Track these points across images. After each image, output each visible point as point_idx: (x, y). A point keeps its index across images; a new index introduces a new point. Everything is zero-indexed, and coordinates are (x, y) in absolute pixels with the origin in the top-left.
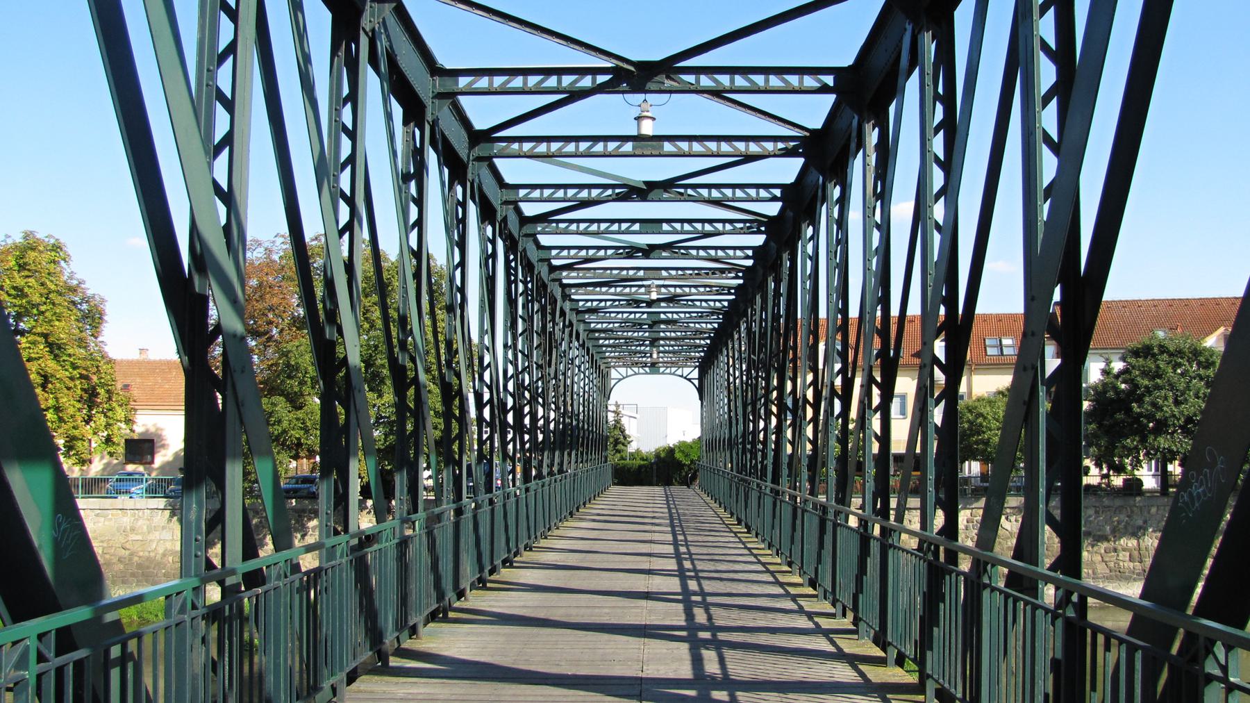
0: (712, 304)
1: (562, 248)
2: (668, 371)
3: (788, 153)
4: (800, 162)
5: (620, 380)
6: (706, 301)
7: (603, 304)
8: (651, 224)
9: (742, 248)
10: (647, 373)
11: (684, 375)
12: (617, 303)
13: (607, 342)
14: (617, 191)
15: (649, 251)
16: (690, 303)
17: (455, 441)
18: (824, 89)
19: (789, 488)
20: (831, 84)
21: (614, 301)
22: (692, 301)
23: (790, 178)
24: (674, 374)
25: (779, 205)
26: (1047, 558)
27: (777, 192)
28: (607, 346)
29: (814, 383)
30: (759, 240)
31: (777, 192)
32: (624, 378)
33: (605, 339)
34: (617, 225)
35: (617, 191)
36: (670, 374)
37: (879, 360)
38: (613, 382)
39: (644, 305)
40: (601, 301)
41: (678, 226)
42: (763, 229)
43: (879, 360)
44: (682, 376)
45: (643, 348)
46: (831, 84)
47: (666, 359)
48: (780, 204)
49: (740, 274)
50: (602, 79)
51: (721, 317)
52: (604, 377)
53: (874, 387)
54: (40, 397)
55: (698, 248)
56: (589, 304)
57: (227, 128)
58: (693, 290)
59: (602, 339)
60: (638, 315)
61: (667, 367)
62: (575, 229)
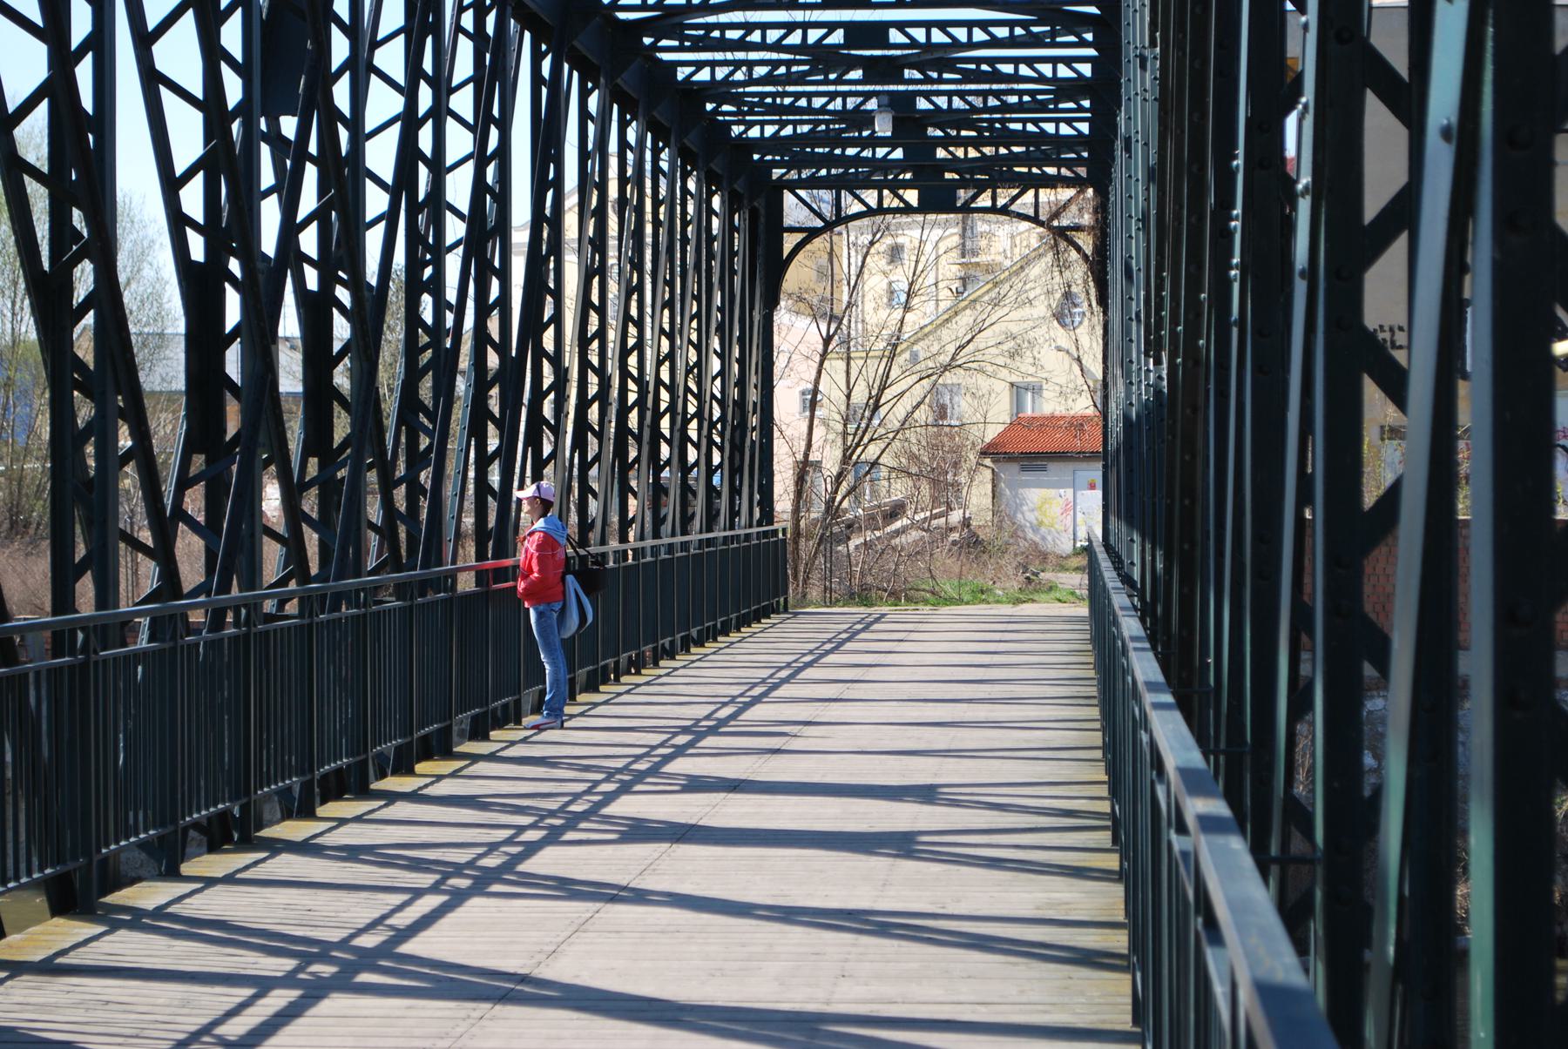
0: (919, 34)
2: (984, 201)
5: (812, 233)
6: (1030, 62)
10: (907, 209)
11: (1043, 217)
16: (984, 67)
17: (592, 459)
24: (1005, 211)
29: (658, 470)
32: (829, 226)
34: (799, 32)
36: (993, 210)
37: (1367, 792)
38: (790, 242)
43: (1367, 792)
44: (1035, 220)
52: (768, 226)
54: (83, 224)
57: (1401, 178)
60: (721, 73)
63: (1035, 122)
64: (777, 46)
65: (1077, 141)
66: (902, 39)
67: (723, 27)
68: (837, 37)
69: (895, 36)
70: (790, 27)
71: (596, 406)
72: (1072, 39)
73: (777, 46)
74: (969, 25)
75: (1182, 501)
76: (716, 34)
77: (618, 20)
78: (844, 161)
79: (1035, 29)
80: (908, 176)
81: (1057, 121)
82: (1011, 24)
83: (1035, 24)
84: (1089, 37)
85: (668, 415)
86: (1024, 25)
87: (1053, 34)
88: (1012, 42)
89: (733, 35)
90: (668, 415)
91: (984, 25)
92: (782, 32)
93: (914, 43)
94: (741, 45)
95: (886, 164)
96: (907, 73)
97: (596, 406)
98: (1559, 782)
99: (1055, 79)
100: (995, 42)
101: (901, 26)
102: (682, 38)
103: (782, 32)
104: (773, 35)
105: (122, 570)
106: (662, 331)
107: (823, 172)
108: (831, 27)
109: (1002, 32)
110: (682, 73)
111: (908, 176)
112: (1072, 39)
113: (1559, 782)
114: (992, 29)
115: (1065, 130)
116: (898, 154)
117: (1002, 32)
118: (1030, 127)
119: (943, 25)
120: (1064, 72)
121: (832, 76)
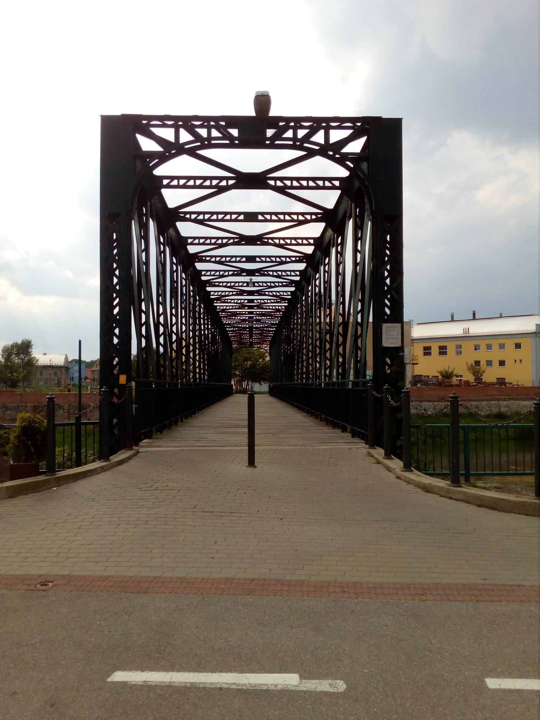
0: (277, 307)
1: (215, 292)
3: (317, 220)
4: (322, 225)
6: (275, 306)
7: (228, 308)
8: (251, 259)
9: (286, 292)
12: (234, 307)
13: (230, 329)
14: (235, 240)
15: (250, 273)
18: (334, 188)
19: (339, 423)
20: (290, 294)
21: (233, 306)
22: (268, 306)
23: (317, 235)
25: (313, 248)
26: (236, 369)
27: (298, 273)
28: (230, 331)
30: (293, 289)
31: (337, 183)
33: (229, 328)
34: (218, 272)
35: (235, 240)
39: (247, 308)
40: (227, 306)
41: (261, 284)
42: (294, 285)
45: (246, 337)
46: (290, 294)
47: (256, 337)
48: (339, 192)
49: (286, 302)
50: (231, 182)
51: (279, 318)
53: (319, 361)
55: (273, 271)
56: (222, 308)
58: (269, 301)
59: (228, 328)
61: (256, 345)
62: (222, 285)
63: (270, 321)
64: (236, 303)
65: (276, 324)
66: (257, 302)
68: (246, 301)
69: (255, 301)
70: (238, 300)
72: (284, 302)
73: (236, 303)
74: (267, 299)
76: (241, 313)
78: (239, 327)
79: (278, 300)
80: (244, 242)
81: (258, 325)
82: (274, 299)
83: (278, 299)
84: (286, 302)
86: (276, 299)
87: (281, 301)
88: (274, 302)
89: (229, 301)
91: (270, 300)
92: (215, 272)
93: (258, 302)
94: (230, 303)
100: (272, 303)
101: (256, 300)
102: (221, 301)
103: (215, 272)
104: (236, 301)
105: (40, 479)
107: (234, 329)
108: (245, 300)
109: (273, 301)
110: (218, 307)
111: (244, 242)
112: (284, 302)
114: (291, 258)
115: (259, 326)
116: (227, 329)
117: (273, 301)
119: (263, 300)
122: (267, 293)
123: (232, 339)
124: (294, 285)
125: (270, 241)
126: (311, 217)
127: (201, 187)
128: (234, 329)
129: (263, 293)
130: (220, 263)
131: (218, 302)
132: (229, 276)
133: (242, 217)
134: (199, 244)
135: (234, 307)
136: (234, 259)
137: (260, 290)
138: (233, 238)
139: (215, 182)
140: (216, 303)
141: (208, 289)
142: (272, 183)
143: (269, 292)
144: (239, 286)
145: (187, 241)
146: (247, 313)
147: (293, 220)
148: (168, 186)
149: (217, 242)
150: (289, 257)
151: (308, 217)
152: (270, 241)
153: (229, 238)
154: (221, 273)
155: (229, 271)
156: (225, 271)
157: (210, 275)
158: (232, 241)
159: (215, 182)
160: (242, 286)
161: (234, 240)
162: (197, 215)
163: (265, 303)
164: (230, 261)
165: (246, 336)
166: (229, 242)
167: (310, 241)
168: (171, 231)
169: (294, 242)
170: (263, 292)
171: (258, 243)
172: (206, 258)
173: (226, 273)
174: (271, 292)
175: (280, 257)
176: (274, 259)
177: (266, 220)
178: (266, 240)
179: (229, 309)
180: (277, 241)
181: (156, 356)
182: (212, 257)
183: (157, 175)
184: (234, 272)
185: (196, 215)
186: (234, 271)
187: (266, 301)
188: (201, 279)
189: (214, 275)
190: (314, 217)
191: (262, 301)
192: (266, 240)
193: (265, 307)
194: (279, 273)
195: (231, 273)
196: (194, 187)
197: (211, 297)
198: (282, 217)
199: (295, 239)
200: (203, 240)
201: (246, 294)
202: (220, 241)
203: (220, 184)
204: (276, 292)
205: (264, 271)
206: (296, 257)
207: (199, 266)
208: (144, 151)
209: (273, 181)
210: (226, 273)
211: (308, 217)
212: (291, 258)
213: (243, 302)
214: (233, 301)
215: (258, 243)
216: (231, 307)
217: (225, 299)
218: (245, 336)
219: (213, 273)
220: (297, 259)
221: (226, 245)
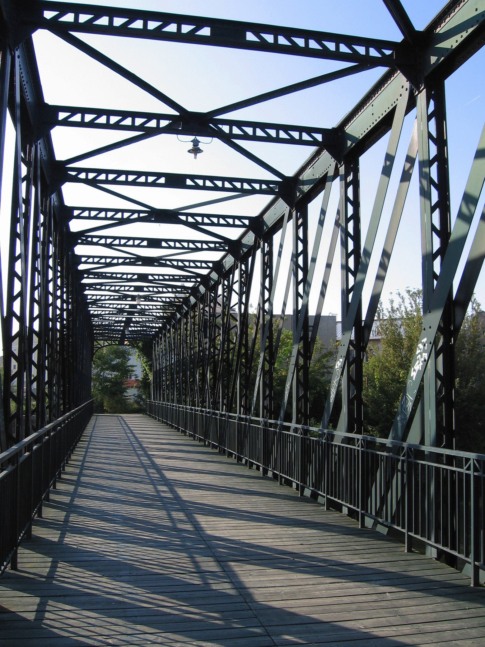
7: (103, 298)
35: (132, 260)
39: (130, 299)
45: (117, 335)
56: (94, 297)
58: (154, 307)
64: (116, 308)
67: (105, 304)
68: (128, 307)
71: (15, 381)
75: (183, 367)
77: (87, 302)
85: (15, 294)
89: (107, 305)
90: (15, 294)
93: (150, 291)
94: (108, 307)
95: (27, 365)
96: (135, 314)
97: (15, 381)
98: (38, 332)
99: (156, 316)
104: (115, 306)
106: (347, 199)
107: (104, 332)
108: (126, 305)
110: (89, 297)
113: (38, 332)
116: (95, 338)
118: (144, 324)
119: (148, 305)
120: (158, 315)
121: (121, 314)
122: (155, 299)
123: (94, 323)
124: (227, 248)
125: (168, 263)
126: (261, 187)
127: (117, 126)
128: (104, 332)
129: (150, 298)
130: (110, 246)
131: (90, 276)
132: (118, 264)
133: (145, 243)
134: (89, 218)
135: (112, 297)
136: (131, 243)
137: (148, 296)
138: (139, 212)
139: (139, 121)
140: (91, 307)
141: (86, 292)
142: (183, 218)
143: (157, 297)
144: (125, 291)
145: (57, 116)
146: (206, 31)
147: (235, 189)
148: (66, 123)
149: (116, 217)
150: (207, 243)
151: (257, 186)
152: (168, 263)
153: (133, 212)
154: (108, 260)
155: (118, 258)
156: (113, 258)
157: (93, 263)
158: (136, 216)
159: (139, 121)
160: (128, 291)
161: (139, 215)
162: (96, 122)
163: (150, 309)
164: (125, 245)
165: (117, 334)
166: (132, 217)
167: (209, 264)
168: (40, 144)
169: (192, 264)
170: (151, 297)
171: (155, 264)
172: (92, 240)
173: (115, 261)
174: (160, 297)
175: (193, 242)
176: (185, 244)
177: (197, 187)
178: (164, 262)
179: (105, 300)
180: (175, 263)
181: (91, 389)
182: (101, 237)
183: (68, 206)
184: (125, 260)
185: (97, 212)
186: (126, 258)
187: (151, 307)
188: (68, 227)
189: (98, 263)
190: (264, 186)
191: (147, 307)
192: (164, 262)
193: (148, 313)
194: (197, 244)
195: (121, 261)
196: (107, 126)
197: (88, 301)
198: (219, 184)
199: (224, 217)
200: (98, 259)
201: (140, 263)
202: (119, 215)
203: (147, 125)
204: (166, 298)
205: (166, 260)
206: (215, 243)
207: (80, 250)
208: (72, 232)
209: (202, 181)
210: (115, 261)
211: (257, 186)
212: (209, 244)
213: (124, 308)
214: (111, 306)
215: (155, 264)
216: (107, 297)
217: (103, 304)
218: (115, 334)
219: (96, 260)
220: (189, 280)
221: (128, 221)
